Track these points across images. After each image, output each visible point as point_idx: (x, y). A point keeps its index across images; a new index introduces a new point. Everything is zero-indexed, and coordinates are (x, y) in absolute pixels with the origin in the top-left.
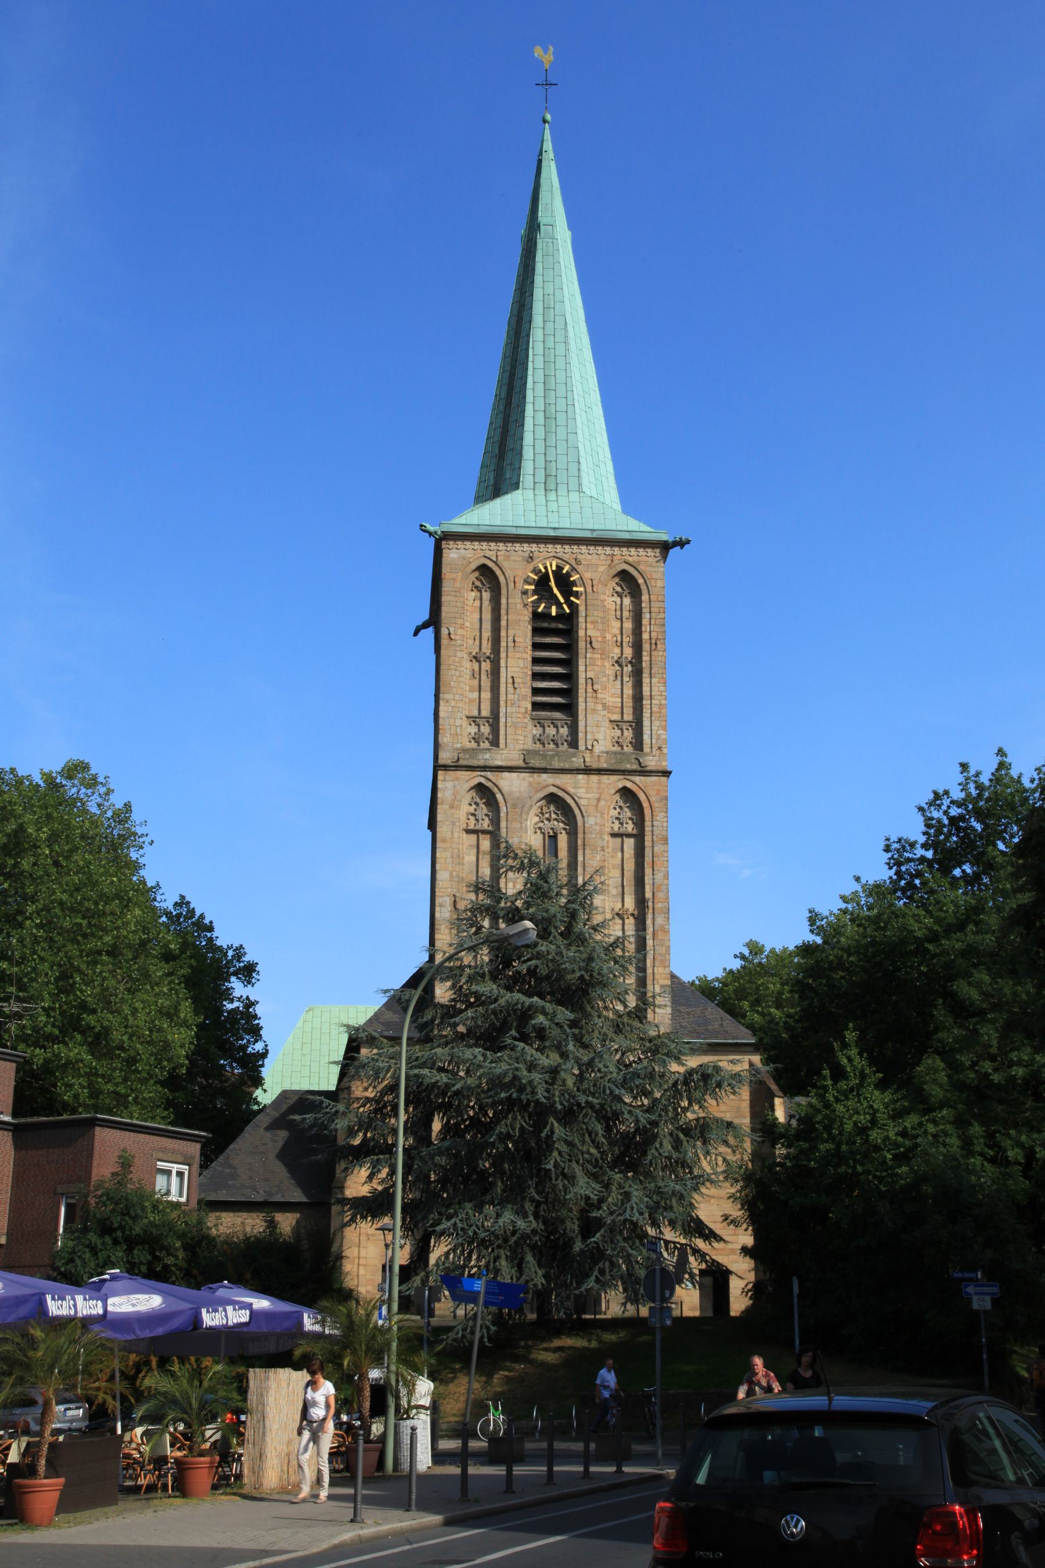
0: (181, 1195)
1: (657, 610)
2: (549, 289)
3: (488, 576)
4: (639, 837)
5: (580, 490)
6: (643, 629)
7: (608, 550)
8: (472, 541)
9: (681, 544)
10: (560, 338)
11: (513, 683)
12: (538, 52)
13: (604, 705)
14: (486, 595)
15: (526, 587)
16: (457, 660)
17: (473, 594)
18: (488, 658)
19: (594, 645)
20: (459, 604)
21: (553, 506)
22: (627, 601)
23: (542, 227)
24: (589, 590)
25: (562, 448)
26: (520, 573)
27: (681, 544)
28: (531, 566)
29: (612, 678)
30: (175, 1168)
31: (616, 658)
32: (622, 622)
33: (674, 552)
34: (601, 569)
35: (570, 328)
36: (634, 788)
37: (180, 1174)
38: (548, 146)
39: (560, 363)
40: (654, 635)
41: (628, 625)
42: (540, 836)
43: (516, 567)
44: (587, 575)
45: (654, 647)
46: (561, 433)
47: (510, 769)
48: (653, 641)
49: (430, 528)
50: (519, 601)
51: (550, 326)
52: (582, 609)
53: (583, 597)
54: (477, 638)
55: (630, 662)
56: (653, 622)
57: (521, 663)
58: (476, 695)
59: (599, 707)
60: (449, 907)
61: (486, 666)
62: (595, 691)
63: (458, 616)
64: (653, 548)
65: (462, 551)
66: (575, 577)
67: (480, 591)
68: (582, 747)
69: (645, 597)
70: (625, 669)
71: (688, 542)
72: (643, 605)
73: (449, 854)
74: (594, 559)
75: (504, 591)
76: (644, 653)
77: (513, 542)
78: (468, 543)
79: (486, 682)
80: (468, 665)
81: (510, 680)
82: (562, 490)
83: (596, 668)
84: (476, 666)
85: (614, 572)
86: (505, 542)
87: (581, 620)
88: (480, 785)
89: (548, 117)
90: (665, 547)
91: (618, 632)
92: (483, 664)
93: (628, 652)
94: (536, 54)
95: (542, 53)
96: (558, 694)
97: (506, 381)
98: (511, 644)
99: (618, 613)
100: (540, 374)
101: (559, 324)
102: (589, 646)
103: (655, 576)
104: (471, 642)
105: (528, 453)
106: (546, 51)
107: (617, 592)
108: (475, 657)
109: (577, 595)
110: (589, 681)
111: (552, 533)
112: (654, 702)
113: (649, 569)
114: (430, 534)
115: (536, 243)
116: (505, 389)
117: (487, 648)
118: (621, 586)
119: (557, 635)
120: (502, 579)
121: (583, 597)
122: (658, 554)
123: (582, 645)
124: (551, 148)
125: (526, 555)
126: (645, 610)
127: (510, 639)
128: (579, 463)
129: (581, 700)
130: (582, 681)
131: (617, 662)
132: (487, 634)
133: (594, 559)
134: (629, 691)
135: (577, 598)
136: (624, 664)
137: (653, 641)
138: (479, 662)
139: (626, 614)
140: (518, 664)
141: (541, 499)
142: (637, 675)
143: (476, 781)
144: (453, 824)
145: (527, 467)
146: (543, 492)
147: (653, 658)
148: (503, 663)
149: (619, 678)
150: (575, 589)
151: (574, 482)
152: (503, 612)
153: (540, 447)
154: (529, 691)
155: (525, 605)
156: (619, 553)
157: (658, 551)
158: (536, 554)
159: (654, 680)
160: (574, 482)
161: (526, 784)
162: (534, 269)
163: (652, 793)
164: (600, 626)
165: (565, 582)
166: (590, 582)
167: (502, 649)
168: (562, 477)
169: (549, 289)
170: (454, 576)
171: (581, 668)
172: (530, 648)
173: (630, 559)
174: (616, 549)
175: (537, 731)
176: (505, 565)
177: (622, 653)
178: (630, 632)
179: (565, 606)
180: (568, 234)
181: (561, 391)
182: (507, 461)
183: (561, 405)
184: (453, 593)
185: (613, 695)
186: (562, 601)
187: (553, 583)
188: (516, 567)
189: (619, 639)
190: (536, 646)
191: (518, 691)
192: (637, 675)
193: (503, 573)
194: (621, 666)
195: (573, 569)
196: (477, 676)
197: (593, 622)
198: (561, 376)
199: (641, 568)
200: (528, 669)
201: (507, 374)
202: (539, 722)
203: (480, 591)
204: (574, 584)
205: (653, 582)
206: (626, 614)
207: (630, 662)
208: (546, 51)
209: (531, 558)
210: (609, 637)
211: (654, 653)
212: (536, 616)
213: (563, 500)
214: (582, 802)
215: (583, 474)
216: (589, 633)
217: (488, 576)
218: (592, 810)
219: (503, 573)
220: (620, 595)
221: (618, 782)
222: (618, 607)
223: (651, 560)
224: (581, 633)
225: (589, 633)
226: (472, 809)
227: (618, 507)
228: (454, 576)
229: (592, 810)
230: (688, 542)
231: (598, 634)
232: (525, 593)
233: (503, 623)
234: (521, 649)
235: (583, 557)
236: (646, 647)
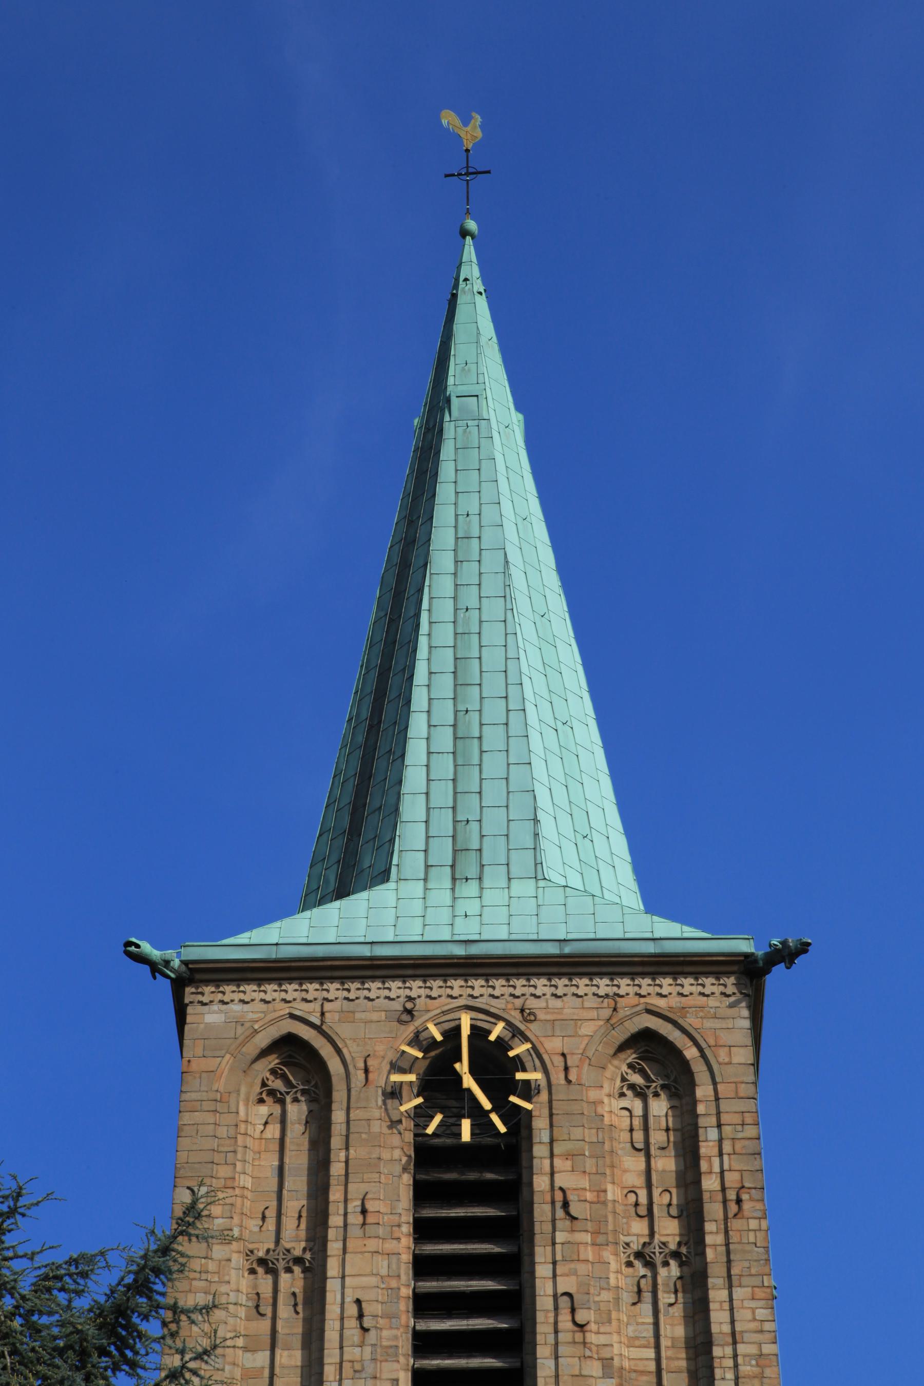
1: (737, 1119)
2: (470, 504)
3: (298, 1063)
5: (538, 874)
6: (704, 1166)
7: (603, 985)
8: (260, 982)
9: (786, 955)
10: (492, 586)
11: (361, 1316)
12: (448, 118)
13: (607, 1363)
14: (297, 1111)
15: (396, 1078)
16: (212, 1266)
17: (264, 1110)
18: (298, 1261)
19: (573, 1210)
20: (222, 1132)
21: (463, 906)
22: (660, 1107)
23: (455, 402)
24: (558, 1077)
25: (494, 793)
26: (380, 1048)
27: (786, 955)
28: (410, 1030)
29: (627, 1297)
31: (635, 1247)
32: (648, 1156)
33: (777, 980)
34: (587, 1029)
35: (516, 574)
38: (471, 269)
39: (493, 634)
40: (732, 1179)
41: (666, 1164)
43: (370, 1036)
44: (552, 1045)
45: (733, 1208)
46: (494, 766)
48: (731, 1195)
49: (146, 948)
50: (377, 1113)
51: (469, 572)
52: (540, 1124)
53: (544, 1096)
54: (271, 1214)
55: (676, 1255)
56: (727, 1147)
57: (382, 1266)
58: (262, 1358)
59: (594, 1368)
61: (292, 1282)
62: (581, 1327)
63: (217, 1158)
64: (718, 975)
65: (236, 1007)
66: (519, 1049)
67: (282, 1102)
69: (703, 1091)
70: (662, 1272)
71: (804, 948)
72: (701, 1109)
75: (339, 1095)
76: (709, 1227)
77: (363, 979)
78: (250, 988)
79: (290, 1323)
80: (245, 1282)
81: (352, 1310)
82: (494, 877)
83: (582, 1268)
84: (265, 1283)
85: (621, 1035)
86: (342, 980)
87: (540, 1151)
89: (472, 225)
90: (750, 973)
91: (638, 1181)
92: (284, 1277)
93: (669, 1230)
94: (444, 122)
95: (457, 122)
97: (371, 686)
98: (355, 1219)
99: (639, 1136)
101: (492, 562)
102: (560, 1213)
103: (725, 1038)
104: (253, 1224)
105: (412, 808)
106: (466, 121)
107: (632, 1087)
108: (262, 1262)
109: (527, 1090)
110: (564, 1302)
112: (741, 1348)
113: (708, 1024)
114: (155, 968)
115: (441, 431)
116: (369, 701)
117: (295, 1239)
118: (643, 1072)
120: (334, 1065)
121: (544, 1096)
122: (730, 989)
123: (542, 1211)
124: (474, 259)
125: (397, 1006)
126: (707, 1122)
127: (354, 1205)
128: (536, 821)
129: (543, 1352)
130: (544, 1302)
131: (639, 1255)
132: (296, 1202)
133: (569, 1007)
134: (674, 1329)
135: (528, 1099)
136: (658, 1259)
137: (731, 1195)
138: (273, 1272)
139: (658, 1137)
142: (695, 1285)
145: (410, 834)
146: (448, 884)
147: (734, 1237)
148: (333, 1268)
149: (647, 1296)
150: (520, 1076)
151: (522, 862)
152: (336, 1142)
153: (442, 795)
154: (405, 1344)
155: (394, 1124)
156: (632, 990)
157: (732, 980)
158: (421, 1003)
159: (738, 1293)
160: (522, 862)
162: (436, 475)
164: (590, 1165)
165: (496, 1066)
166: (559, 1061)
167: (331, 1234)
168: (494, 851)
169: (470, 504)
170: (212, 1064)
171: (543, 1270)
172: (407, 1229)
173: (661, 1003)
174: (624, 982)
176: (343, 1031)
177: (652, 1234)
178: (671, 1181)
179: (494, 1118)
180: (516, 420)
181: (494, 685)
182: (367, 832)
183: (494, 711)
184: (207, 1106)
185: (632, 1342)
186: (487, 1105)
187: (463, 1067)
188: (370, 1036)
189: (643, 1199)
190: (424, 1230)
191: (372, 1336)
192: (695, 1285)
193: (339, 1051)
194: (650, 1264)
195: (518, 1034)
196: (268, 1311)
197: (569, 1156)
198: (493, 658)
199: (691, 1021)
201: (374, 674)
203: (282, 1102)
204: (519, 1064)
205: (723, 1055)
206: (658, 1137)
207: (676, 1255)
208: (466, 121)
209: (410, 1012)
210: (613, 1192)
211: (735, 1224)
212: (425, 1155)
215: (544, 844)
216: (559, 1181)
217: (298, 1063)
219: (339, 1051)
220: (640, 1093)
222: (637, 1122)
223: (712, 1002)
224: (541, 1183)
225: (559, 1181)
227: (633, 899)
228: (212, 1064)
230: (804, 948)
231: (585, 1183)
232: (394, 1093)
233: (337, 1169)
234: (381, 1231)
235: (541, 1003)
236: (713, 1210)
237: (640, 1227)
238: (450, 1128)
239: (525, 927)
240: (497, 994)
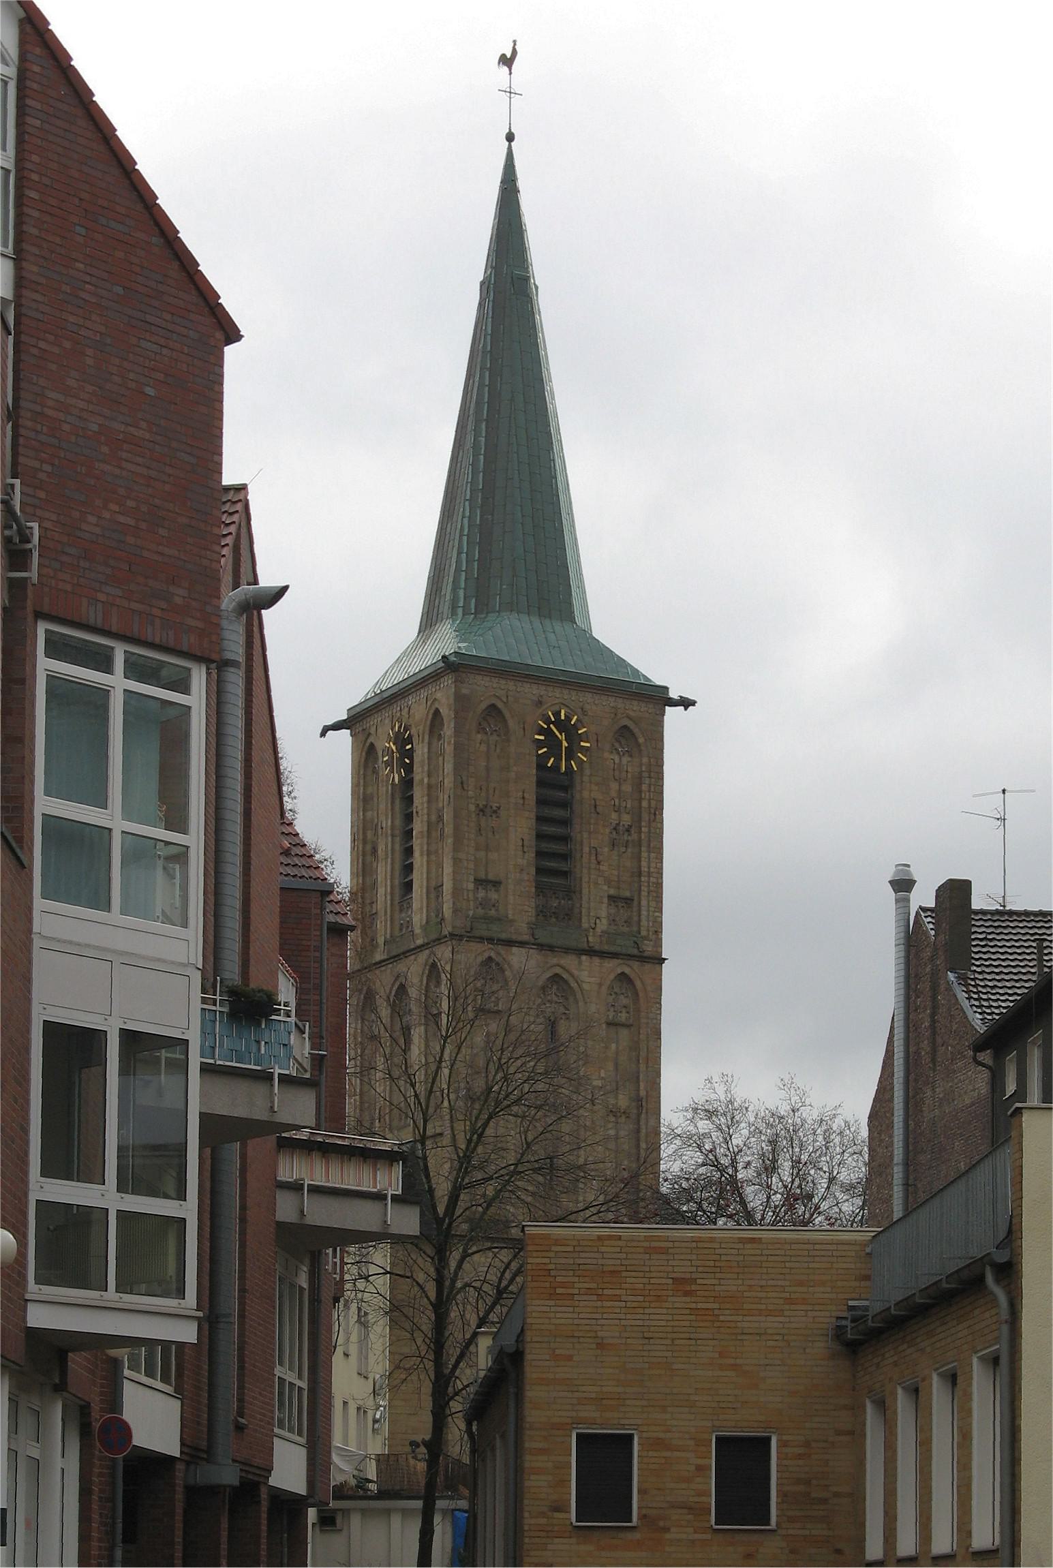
9: (686, 703)
36: (632, 976)
47: (522, 944)
52: (586, 766)
59: (601, 880)
71: (693, 703)
130: (586, 849)
212: (541, 766)
214: (586, 986)
230: (693, 703)
240: (572, 697)
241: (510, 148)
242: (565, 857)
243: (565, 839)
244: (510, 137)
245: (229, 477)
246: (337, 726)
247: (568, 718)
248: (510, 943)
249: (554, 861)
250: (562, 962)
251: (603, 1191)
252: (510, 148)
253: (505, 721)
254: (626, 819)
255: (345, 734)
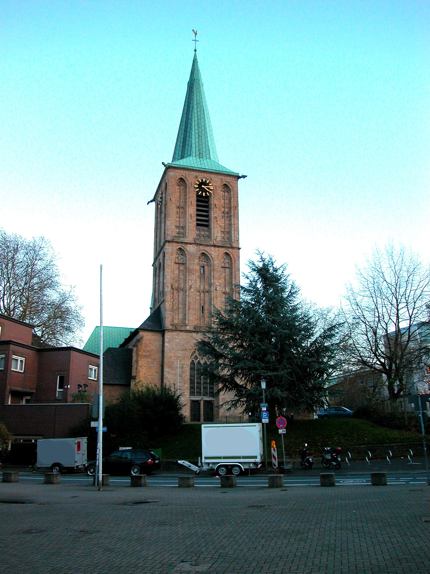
0: (206, 458)
4: (230, 268)
5: (210, 159)
9: (244, 177)
10: (202, 113)
21: (202, 162)
25: (204, 145)
28: (197, 180)
30: (20, 358)
34: (219, 183)
36: (229, 253)
37: (22, 361)
42: (199, 266)
43: (192, 180)
47: (191, 244)
52: (212, 194)
59: (218, 226)
60: (170, 288)
68: (213, 239)
71: (246, 176)
73: (170, 270)
74: (216, 179)
84: (178, 210)
88: (180, 248)
96: (204, 221)
100: (196, 123)
111: (203, 170)
119: (203, 202)
123: (212, 206)
130: (213, 217)
133: (216, 179)
140: (192, 210)
141: (198, 160)
143: (179, 247)
144: (171, 260)
160: (208, 156)
161: (195, 249)
163: (235, 255)
168: (204, 154)
169: (198, 98)
175: (198, 232)
176: (188, 178)
190: (198, 206)
198: (203, 124)
199: (231, 184)
200: (195, 213)
202: (198, 230)
212: (198, 196)
213: (205, 161)
214: (213, 256)
218: (216, 258)
220: (224, 192)
221: (223, 250)
224: (212, 202)
226: (177, 256)
229: (216, 258)
230: (246, 176)
237: (223, 209)
238: (202, 193)
239: (210, 167)
240: (208, 176)
241: (195, 56)
242: (207, 221)
243: (207, 216)
244: (195, 51)
245: (144, 390)
246: (151, 201)
247: (206, 181)
248: (187, 243)
249: (204, 221)
250: (205, 249)
251: (329, 375)
252: (195, 56)
253: (185, 182)
254: (227, 210)
255: (154, 202)
